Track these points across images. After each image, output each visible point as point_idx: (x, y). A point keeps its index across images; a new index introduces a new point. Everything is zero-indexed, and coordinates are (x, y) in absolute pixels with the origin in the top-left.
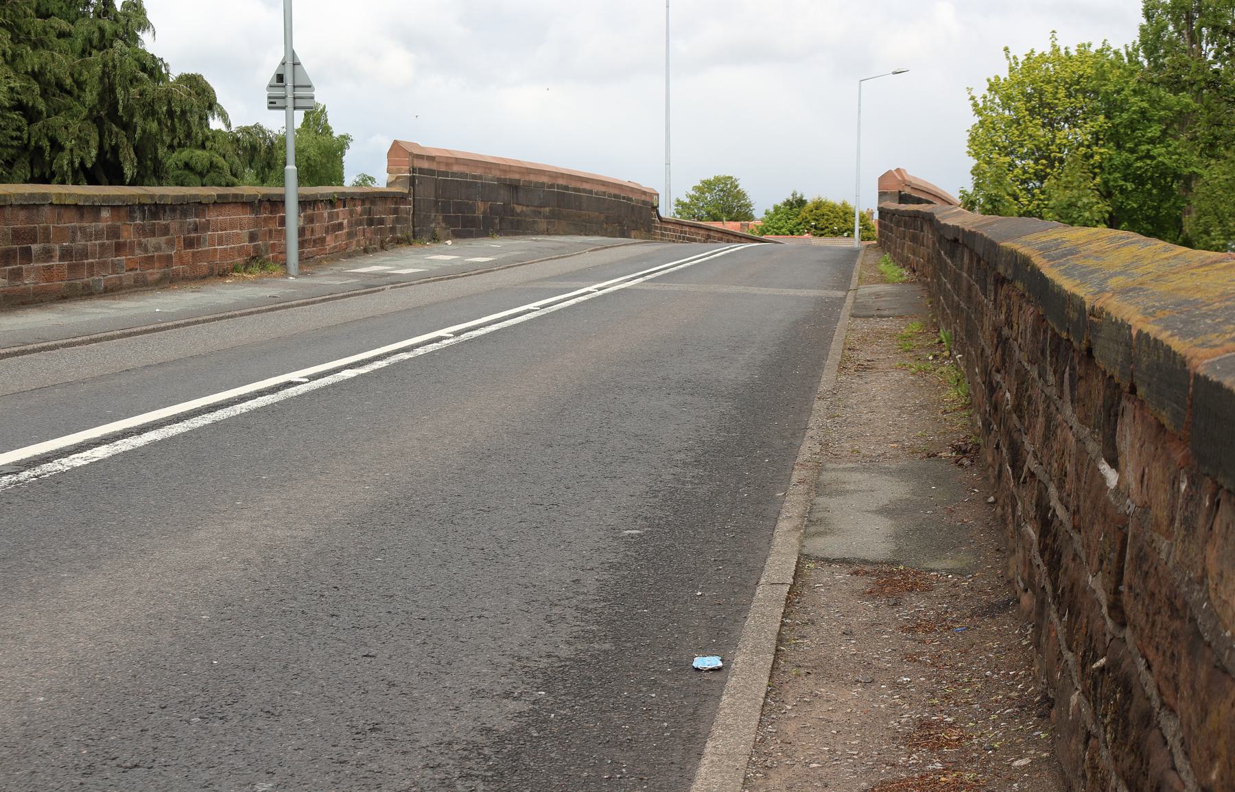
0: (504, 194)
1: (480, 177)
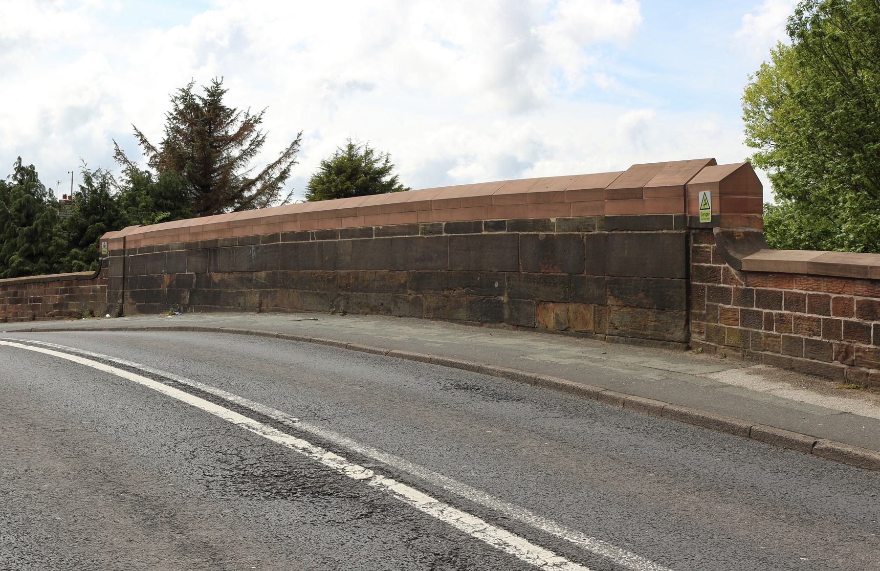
0: (197, 262)
1: (166, 247)
